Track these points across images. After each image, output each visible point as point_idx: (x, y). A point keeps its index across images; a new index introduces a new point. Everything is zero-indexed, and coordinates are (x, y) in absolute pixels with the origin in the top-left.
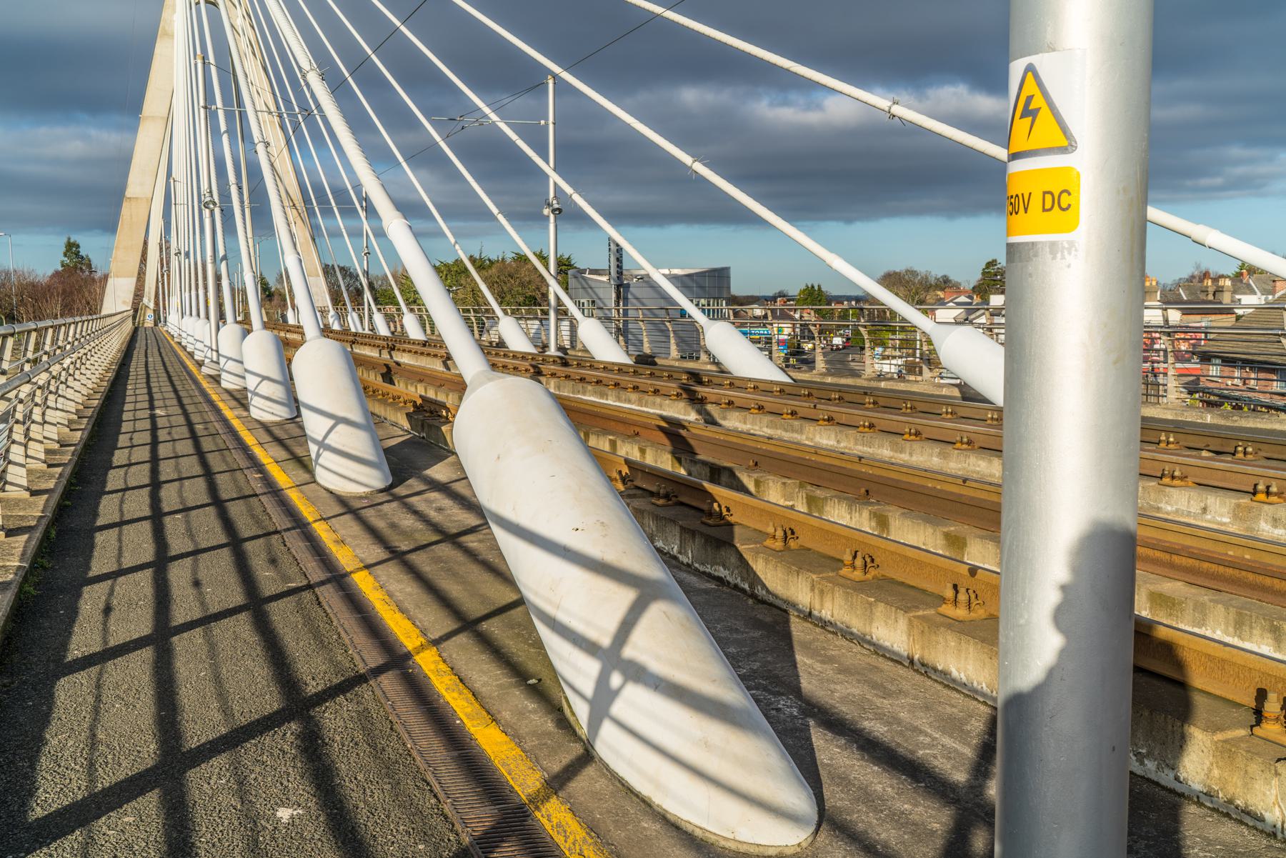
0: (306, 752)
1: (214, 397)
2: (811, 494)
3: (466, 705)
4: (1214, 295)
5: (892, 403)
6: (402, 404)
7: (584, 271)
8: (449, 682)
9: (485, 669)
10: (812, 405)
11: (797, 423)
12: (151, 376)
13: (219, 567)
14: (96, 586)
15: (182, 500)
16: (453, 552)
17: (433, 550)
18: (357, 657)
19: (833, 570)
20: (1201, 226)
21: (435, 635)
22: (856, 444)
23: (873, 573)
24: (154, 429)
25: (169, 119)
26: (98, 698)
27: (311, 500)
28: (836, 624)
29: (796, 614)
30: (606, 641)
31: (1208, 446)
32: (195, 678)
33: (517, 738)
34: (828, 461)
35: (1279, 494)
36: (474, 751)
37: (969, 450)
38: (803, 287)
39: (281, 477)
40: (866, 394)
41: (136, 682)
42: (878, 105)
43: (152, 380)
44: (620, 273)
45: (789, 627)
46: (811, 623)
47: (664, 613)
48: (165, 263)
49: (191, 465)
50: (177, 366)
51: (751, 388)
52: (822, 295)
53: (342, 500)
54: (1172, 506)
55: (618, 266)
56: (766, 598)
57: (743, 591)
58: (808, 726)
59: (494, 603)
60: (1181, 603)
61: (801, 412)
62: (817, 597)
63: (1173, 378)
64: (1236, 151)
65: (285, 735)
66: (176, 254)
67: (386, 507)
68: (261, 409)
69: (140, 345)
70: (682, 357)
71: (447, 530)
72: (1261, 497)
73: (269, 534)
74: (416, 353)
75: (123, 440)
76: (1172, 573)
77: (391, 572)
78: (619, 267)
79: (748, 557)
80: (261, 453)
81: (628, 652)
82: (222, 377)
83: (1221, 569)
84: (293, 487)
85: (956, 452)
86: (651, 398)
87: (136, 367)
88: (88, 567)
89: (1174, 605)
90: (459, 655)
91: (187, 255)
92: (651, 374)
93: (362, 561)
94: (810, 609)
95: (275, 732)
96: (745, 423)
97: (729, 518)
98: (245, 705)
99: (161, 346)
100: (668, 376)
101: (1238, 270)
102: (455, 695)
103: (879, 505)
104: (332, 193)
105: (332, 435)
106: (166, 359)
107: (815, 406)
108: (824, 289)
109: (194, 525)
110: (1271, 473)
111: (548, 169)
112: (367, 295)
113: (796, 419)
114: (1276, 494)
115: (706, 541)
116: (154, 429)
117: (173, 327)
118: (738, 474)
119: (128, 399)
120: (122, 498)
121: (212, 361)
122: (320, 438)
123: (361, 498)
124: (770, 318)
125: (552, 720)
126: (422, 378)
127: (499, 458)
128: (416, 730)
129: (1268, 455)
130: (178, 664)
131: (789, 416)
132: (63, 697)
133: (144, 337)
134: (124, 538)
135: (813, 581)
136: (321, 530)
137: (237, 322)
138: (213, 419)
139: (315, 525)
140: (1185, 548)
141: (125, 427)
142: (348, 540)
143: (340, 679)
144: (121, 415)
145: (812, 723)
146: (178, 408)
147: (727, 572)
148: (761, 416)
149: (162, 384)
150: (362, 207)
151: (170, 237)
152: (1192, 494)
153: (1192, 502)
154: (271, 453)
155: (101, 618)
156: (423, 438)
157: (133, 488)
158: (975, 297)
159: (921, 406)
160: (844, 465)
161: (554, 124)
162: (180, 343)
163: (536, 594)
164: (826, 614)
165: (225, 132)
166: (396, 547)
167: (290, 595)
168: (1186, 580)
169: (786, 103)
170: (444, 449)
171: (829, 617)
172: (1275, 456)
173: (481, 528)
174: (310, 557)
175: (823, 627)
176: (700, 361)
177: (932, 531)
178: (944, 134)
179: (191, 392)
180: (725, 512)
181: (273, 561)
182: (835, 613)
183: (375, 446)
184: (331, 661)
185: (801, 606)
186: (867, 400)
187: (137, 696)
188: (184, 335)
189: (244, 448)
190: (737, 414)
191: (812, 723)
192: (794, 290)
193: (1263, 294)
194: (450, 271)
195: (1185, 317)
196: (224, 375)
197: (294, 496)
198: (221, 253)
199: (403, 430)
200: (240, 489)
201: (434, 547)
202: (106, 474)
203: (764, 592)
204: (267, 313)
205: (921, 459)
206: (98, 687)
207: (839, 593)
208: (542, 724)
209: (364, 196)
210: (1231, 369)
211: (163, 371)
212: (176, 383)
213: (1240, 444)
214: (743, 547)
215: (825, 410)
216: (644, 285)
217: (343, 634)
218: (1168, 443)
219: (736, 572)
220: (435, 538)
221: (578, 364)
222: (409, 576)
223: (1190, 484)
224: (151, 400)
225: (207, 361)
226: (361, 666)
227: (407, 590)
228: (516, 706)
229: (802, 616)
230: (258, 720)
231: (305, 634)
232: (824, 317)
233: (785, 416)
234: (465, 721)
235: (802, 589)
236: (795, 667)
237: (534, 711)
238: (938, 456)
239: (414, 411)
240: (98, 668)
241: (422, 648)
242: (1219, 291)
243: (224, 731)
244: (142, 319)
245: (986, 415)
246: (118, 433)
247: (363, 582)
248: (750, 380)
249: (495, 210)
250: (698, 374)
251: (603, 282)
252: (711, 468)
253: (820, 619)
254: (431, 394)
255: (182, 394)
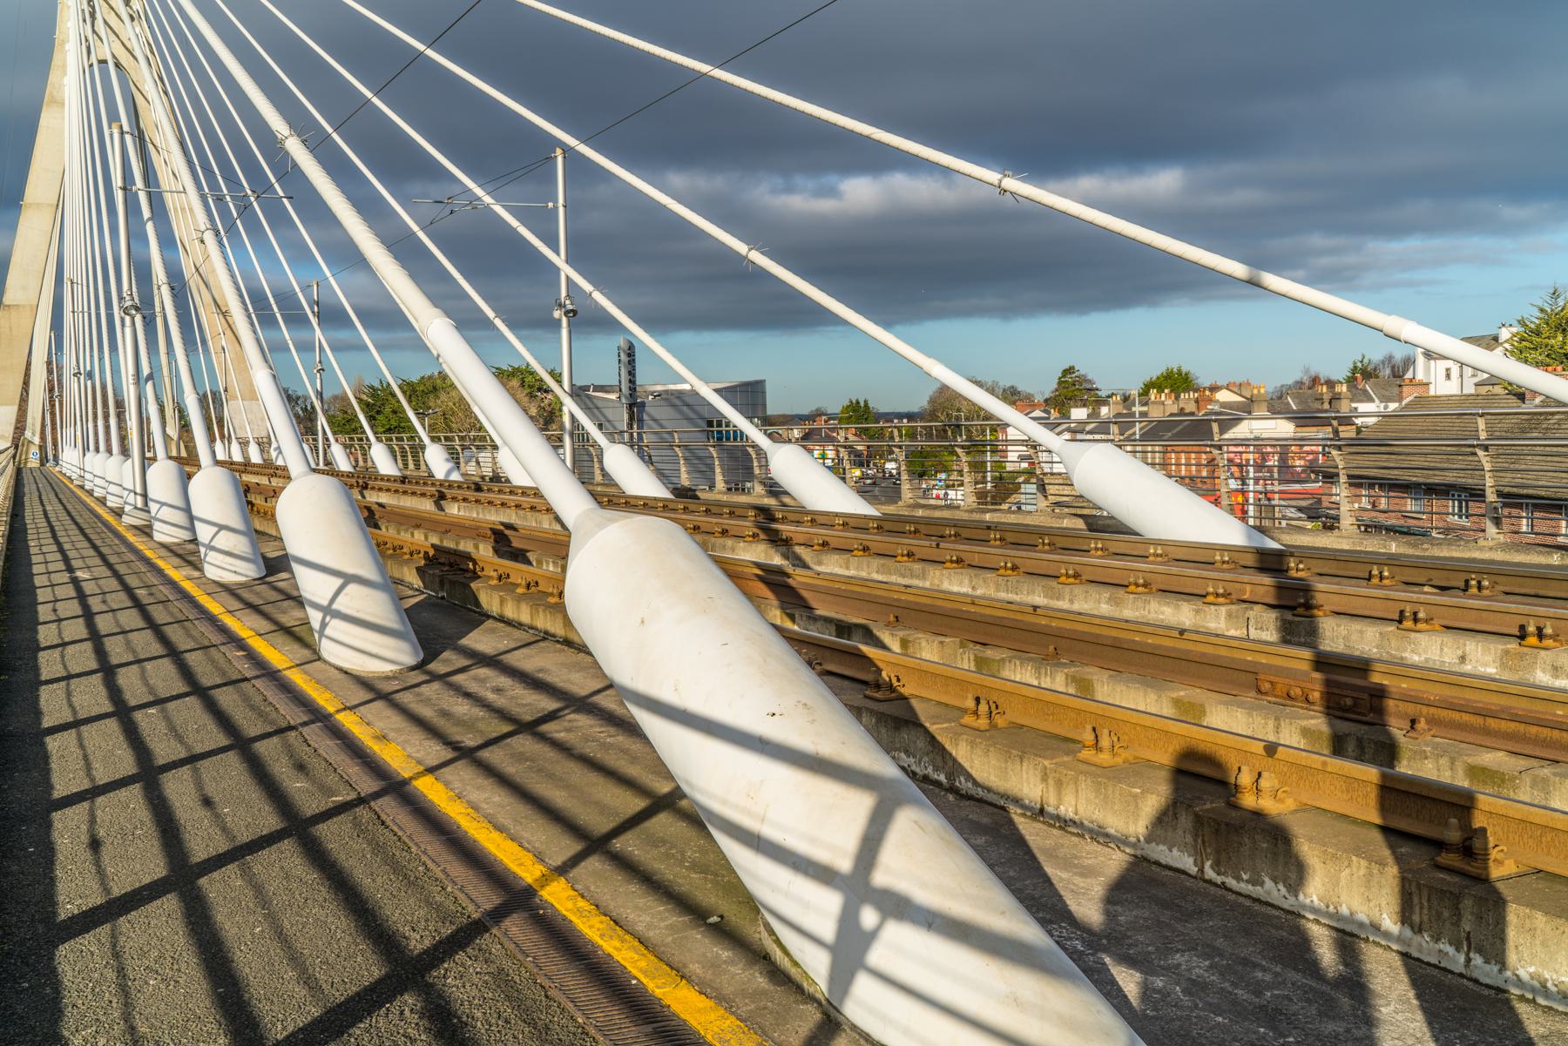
0: (442, 1037)
1: (149, 554)
2: (981, 655)
3: (636, 957)
4: (1330, 403)
5: (1024, 539)
6: (407, 557)
7: (586, 388)
8: (601, 926)
9: (641, 905)
10: (934, 544)
11: (917, 567)
12: (56, 528)
13: (228, 775)
14: (69, 811)
15: (151, 690)
16: (536, 746)
17: (509, 744)
18: (461, 896)
19: (1067, 754)
20: (1393, 317)
21: (558, 861)
22: (998, 590)
23: (1123, 756)
24: (82, 597)
25: (59, 204)
26: (121, 971)
27: (324, 684)
28: (1082, 823)
29: (1019, 811)
30: (845, 864)
31: (1431, 580)
32: (249, 937)
33: (720, 999)
34: (988, 611)
35: (1555, 637)
36: (673, 1023)
37: (1145, 593)
38: (847, 403)
39: (276, 655)
40: (989, 528)
41: (168, 947)
42: (984, 178)
43: (59, 534)
44: (633, 389)
45: (1017, 830)
46: (1044, 823)
47: (916, 822)
48: (53, 389)
49: (146, 643)
50: (87, 515)
51: (839, 525)
52: (869, 412)
53: (363, 682)
54: (1420, 655)
55: (630, 381)
56: (974, 792)
57: (938, 784)
58: (1105, 964)
59: (618, 814)
60: (1513, 779)
61: (919, 553)
62: (1051, 789)
63: (1347, 500)
64: (1317, 240)
65: (402, 1013)
66: (75, 375)
67: (424, 689)
68: (219, 567)
69: (29, 489)
70: (729, 489)
71: (518, 717)
72: (1533, 640)
73: (280, 731)
74: (396, 491)
75: (44, 612)
76: (1488, 741)
77: (462, 773)
78: (632, 381)
79: (943, 739)
80: (236, 625)
81: (880, 878)
82: (154, 527)
83: (1556, 734)
84: (293, 667)
85: (1131, 596)
86: (721, 541)
87: (33, 515)
88: (49, 787)
89: (1503, 781)
90: (598, 887)
91: (90, 375)
92: (706, 511)
93: (419, 762)
94: (1042, 805)
95: (388, 1009)
96: (848, 568)
97: (902, 690)
98: (333, 973)
99: (58, 490)
100: (730, 513)
101: (1349, 374)
102: (617, 944)
103: (1075, 666)
104: (274, 297)
105: (340, 599)
106: (69, 507)
107: (938, 545)
108: (871, 405)
109: (178, 721)
110: (1541, 611)
111: (559, 261)
112: (322, 421)
113: (914, 561)
114: (1551, 637)
115: (879, 721)
116: (82, 597)
117: (69, 466)
118: (877, 633)
119: (35, 559)
120: (67, 689)
121: (136, 508)
122: (325, 603)
123: (387, 678)
124: (897, 439)
125: (761, 973)
126: (419, 522)
127: (643, 622)
128: (581, 996)
129: (1507, 589)
130: (219, 918)
131: (906, 558)
132: (70, 973)
133: (32, 480)
134: (86, 743)
135: (1046, 768)
136: (347, 721)
137: (170, 458)
138: (156, 583)
139: (340, 717)
140: (1504, 709)
141: (42, 595)
142: (392, 735)
143: (448, 930)
144: (32, 580)
145: (1107, 960)
146: (104, 568)
147: (912, 760)
148: (869, 559)
149: (73, 539)
150: (313, 312)
151: (62, 354)
152: (1445, 639)
153: (1445, 650)
154: (248, 624)
155: (88, 855)
156: (443, 598)
157: (79, 675)
158: (1052, 411)
159: (1061, 542)
160: (1012, 616)
161: (565, 206)
162: (82, 487)
163: (724, 802)
164: (1067, 810)
165: (149, 219)
166: (458, 742)
167: (340, 814)
168: (1510, 749)
169: (790, 190)
170: (475, 612)
171: (1071, 815)
172: (1517, 590)
173: (562, 714)
174: (348, 761)
175: (1061, 828)
176: (716, 490)
177: (1156, 697)
178: (1082, 216)
179: (115, 548)
180: (895, 683)
181: (301, 767)
182: (1081, 810)
183: (398, 608)
184: (428, 903)
185: (1027, 802)
186: (948, 532)
187: (176, 967)
188: (88, 476)
189: (212, 619)
190: (837, 557)
191: (1107, 960)
192: (835, 407)
193: (1381, 402)
194: (414, 391)
195: (1299, 429)
196: (157, 525)
197: (297, 678)
198: (146, 371)
199: (412, 589)
200: (224, 673)
201: (509, 740)
202: (36, 659)
203: (970, 785)
204: (186, 447)
205: (1086, 606)
206: (117, 955)
207: (1085, 785)
208: (749, 980)
209: (316, 298)
210: (1329, 485)
211: (70, 522)
212: (93, 537)
213: (1473, 576)
214: (935, 727)
215: (950, 549)
216: (662, 403)
217: (430, 864)
218: (1381, 578)
219: (926, 759)
220: (506, 728)
221: (609, 501)
222: (491, 780)
223: (1437, 627)
224: (66, 560)
225: (128, 508)
226: (471, 908)
227: (495, 800)
228: (704, 955)
229: (1029, 814)
230: (358, 994)
231: (380, 867)
232: (871, 438)
233: (899, 558)
234: (645, 980)
235: (1028, 778)
236: (1051, 884)
237: (732, 962)
238: (1107, 603)
239: (425, 565)
240: (107, 927)
241: (545, 880)
242: (1335, 398)
243: (316, 1012)
244: (23, 457)
245: (1147, 550)
246: (35, 603)
247: (431, 790)
248: (837, 515)
249: (490, 314)
250: (768, 509)
251: (612, 400)
252: (836, 625)
253: (1058, 818)
254: (449, 544)
255: (105, 550)
